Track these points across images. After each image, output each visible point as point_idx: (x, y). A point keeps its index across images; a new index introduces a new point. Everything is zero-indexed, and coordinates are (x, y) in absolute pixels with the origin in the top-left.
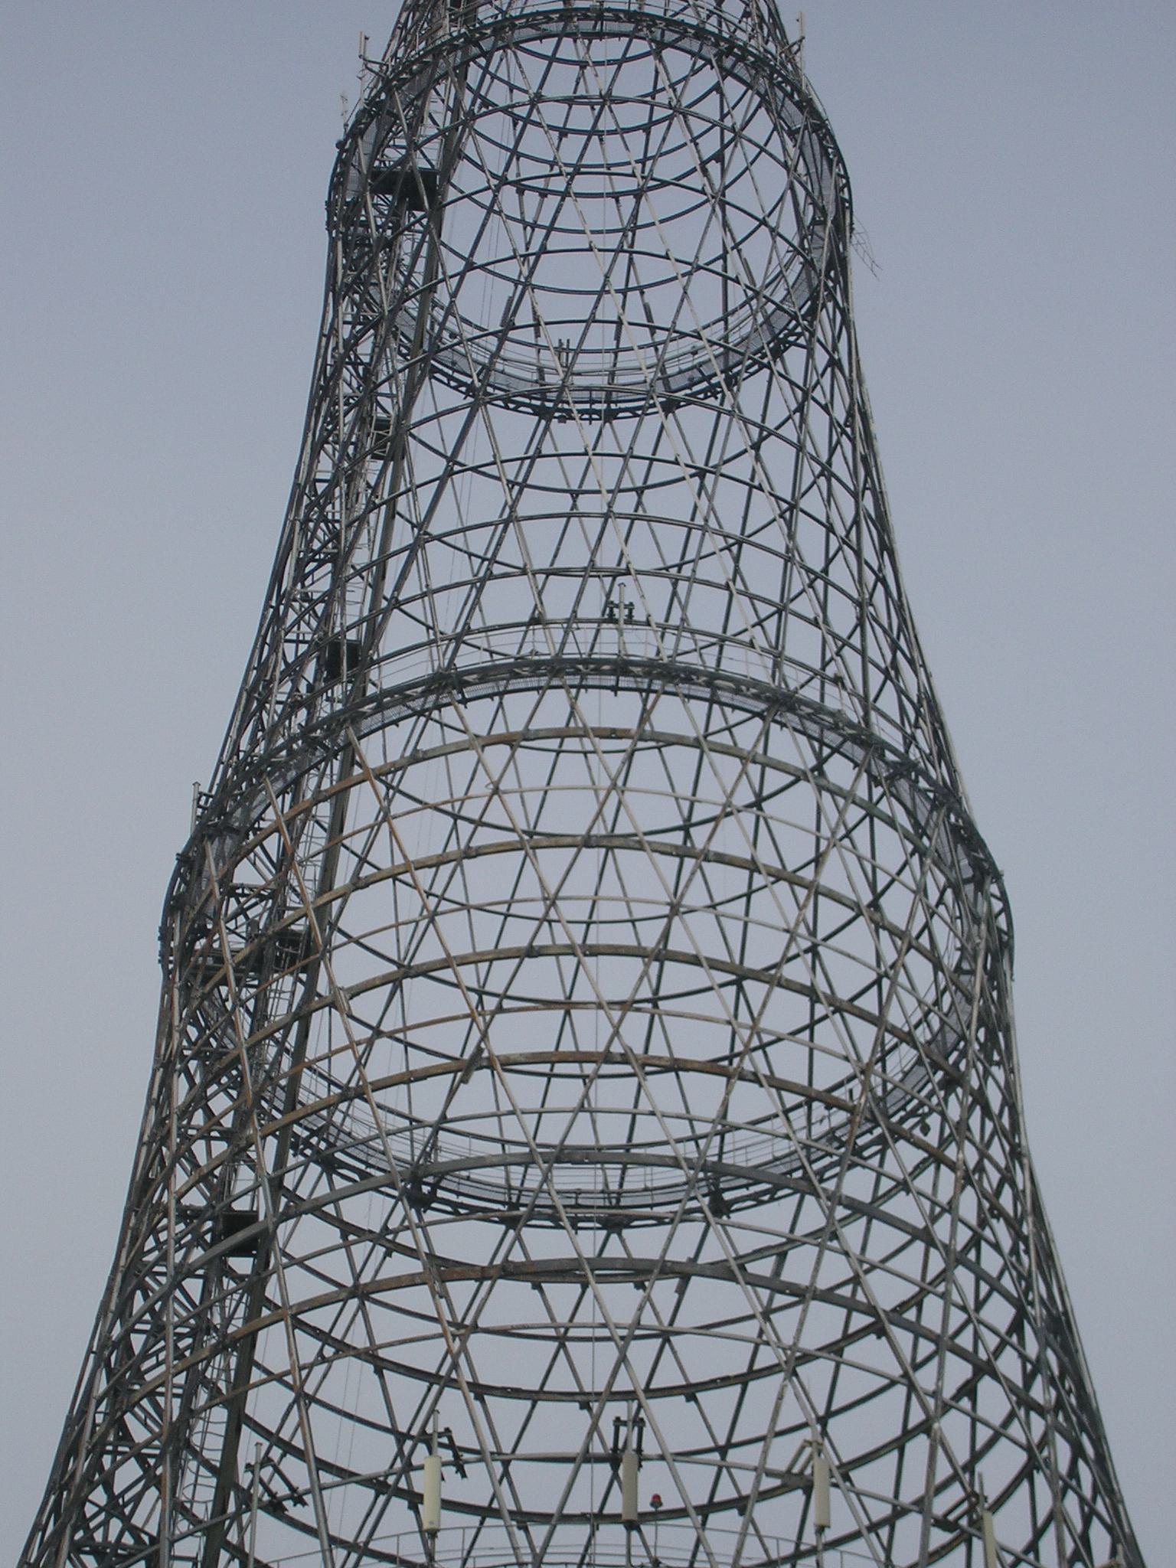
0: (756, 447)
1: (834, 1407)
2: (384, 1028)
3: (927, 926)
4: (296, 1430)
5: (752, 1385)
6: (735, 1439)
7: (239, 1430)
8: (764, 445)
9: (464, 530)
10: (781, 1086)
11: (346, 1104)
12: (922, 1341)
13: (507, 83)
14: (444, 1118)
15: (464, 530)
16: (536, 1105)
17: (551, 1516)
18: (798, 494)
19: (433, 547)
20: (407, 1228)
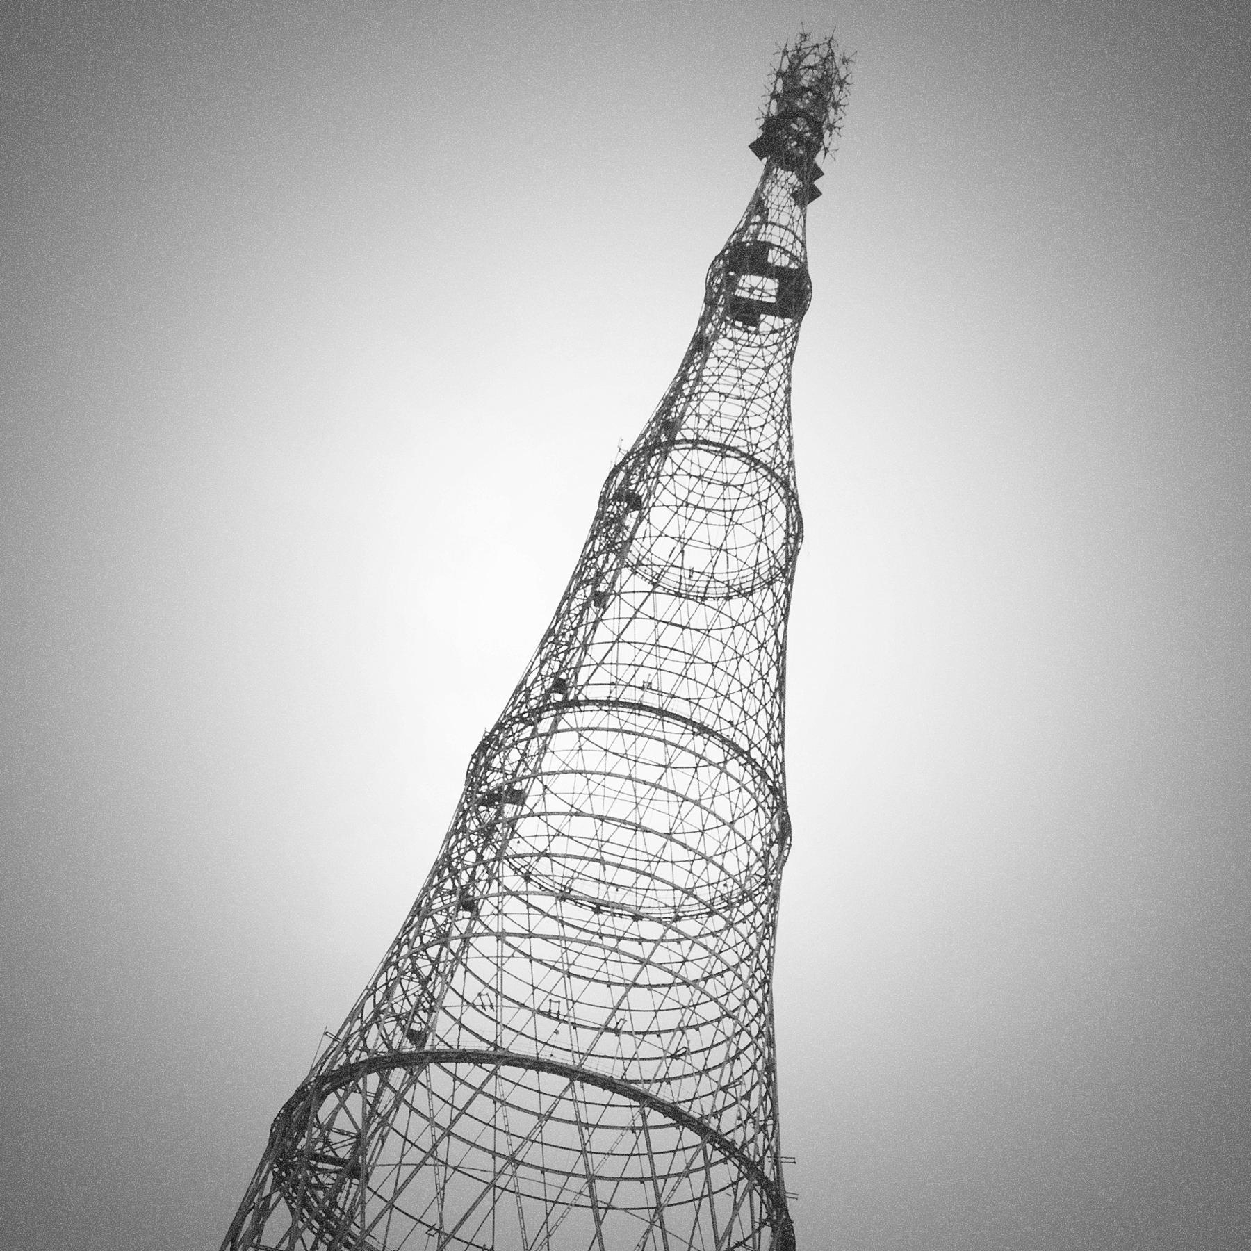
0: (733, 627)
1: (647, 594)
2: (675, 511)
3: (528, 740)
4: (624, 585)
5: (596, 1129)
6: (647, 594)
7: (565, 1075)
8: (736, 628)
9: (717, 827)
10: (423, 1163)
11: (704, 976)
12: (606, 951)
13: (697, 682)
14: (720, 717)
15: (717, 827)
16: (706, 467)
17: (649, 1080)
18: (765, 641)
19: (671, 474)
20: (719, 768)
